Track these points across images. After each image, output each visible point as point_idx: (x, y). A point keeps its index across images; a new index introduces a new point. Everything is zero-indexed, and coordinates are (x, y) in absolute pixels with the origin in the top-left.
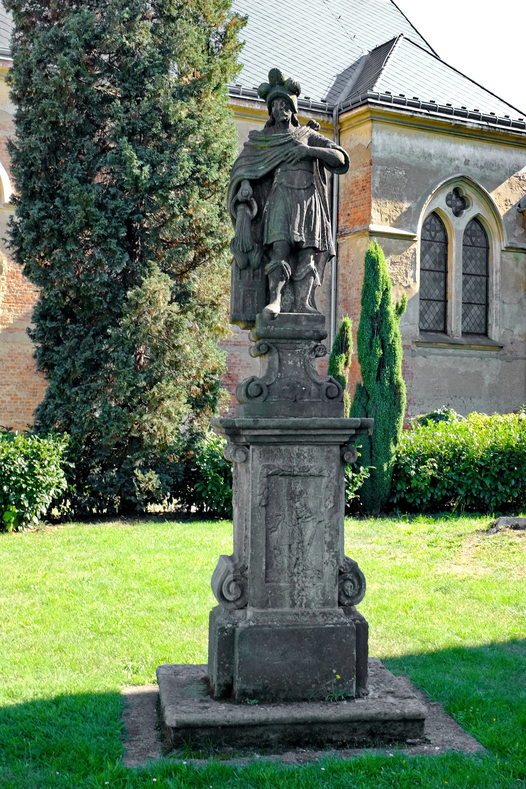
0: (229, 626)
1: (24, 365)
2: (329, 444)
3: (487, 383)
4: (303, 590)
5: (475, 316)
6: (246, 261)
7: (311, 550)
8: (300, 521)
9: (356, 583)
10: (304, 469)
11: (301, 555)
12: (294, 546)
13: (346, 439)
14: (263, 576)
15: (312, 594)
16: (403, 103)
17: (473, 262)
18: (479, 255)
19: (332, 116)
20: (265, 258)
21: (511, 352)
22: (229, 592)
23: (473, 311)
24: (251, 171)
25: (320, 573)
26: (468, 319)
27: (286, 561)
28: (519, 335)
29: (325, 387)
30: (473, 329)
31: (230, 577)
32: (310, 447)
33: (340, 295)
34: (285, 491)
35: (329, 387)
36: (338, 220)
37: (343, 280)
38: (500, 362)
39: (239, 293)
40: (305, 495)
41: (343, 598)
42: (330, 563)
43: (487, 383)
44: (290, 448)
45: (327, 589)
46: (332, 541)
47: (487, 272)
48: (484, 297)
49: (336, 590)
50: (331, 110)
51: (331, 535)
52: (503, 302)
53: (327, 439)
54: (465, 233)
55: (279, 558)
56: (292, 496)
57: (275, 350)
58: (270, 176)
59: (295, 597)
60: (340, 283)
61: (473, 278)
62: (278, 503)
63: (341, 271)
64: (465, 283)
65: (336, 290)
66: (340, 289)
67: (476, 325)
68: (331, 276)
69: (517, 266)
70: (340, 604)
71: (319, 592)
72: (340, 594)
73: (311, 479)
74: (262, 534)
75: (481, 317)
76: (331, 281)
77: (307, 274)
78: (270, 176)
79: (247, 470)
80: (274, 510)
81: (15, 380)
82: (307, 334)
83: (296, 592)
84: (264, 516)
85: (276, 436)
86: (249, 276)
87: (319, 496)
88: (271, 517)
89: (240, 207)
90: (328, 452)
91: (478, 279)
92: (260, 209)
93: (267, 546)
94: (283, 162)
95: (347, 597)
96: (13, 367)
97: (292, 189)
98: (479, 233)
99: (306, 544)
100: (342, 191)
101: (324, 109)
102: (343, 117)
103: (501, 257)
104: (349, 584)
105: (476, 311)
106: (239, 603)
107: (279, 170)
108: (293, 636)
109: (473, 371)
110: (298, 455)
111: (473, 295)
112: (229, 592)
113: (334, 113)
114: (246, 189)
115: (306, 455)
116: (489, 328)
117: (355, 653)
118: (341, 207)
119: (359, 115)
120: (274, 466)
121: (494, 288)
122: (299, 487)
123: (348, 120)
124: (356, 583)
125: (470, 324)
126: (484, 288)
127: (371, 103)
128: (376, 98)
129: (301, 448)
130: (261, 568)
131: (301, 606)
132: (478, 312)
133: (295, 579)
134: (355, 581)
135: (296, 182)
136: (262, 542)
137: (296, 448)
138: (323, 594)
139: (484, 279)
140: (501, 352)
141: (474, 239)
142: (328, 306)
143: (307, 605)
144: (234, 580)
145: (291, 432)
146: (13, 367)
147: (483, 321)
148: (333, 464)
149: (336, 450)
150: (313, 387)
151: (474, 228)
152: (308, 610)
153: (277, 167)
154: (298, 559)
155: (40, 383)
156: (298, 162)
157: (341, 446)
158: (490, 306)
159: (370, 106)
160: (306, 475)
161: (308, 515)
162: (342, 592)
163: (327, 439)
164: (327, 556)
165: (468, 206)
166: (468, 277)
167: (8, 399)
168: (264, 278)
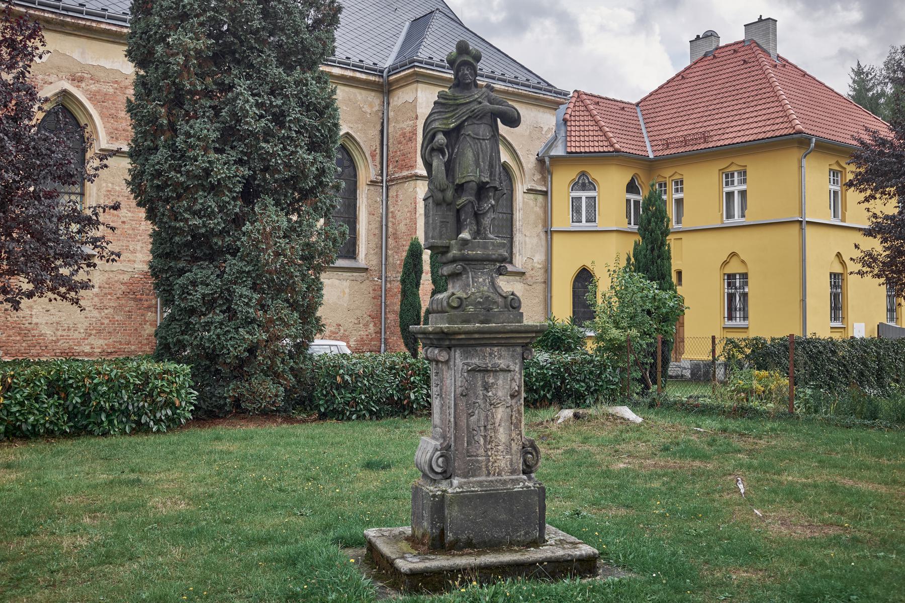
0: (439, 493)
1: (120, 291)
7: (501, 430)
10: (494, 365)
12: (489, 427)
16: (432, 65)
24: (444, 124)
29: (509, 299)
33: (390, 230)
34: (480, 383)
36: (388, 166)
44: (484, 348)
47: (512, 211)
50: (382, 72)
53: (512, 341)
56: (486, 387)
62: (475, 393)
63: (391, 209)
66: (390, 224)
78: (458, 128)
81: (112, 304)
82: (493, 257)
92: (450, 155)
94: (470, 117)
96: (110, 294)
100: (391, 141)
108: (491, 498)
113: (385, 74)
118: (391, 154)
122: (491, 380)
128: (421, 62)
131: (494, 475)
133: (490, 453)
137: (488, 349)
138: (511, 465)
139: (509, 216)
143: (499, 474)
145: (477, 336)
146: (110, 294)
150: (500, 300)
152: (500, 478)
160: (496, 371)
163: (512, 341)
167: (106, 321)
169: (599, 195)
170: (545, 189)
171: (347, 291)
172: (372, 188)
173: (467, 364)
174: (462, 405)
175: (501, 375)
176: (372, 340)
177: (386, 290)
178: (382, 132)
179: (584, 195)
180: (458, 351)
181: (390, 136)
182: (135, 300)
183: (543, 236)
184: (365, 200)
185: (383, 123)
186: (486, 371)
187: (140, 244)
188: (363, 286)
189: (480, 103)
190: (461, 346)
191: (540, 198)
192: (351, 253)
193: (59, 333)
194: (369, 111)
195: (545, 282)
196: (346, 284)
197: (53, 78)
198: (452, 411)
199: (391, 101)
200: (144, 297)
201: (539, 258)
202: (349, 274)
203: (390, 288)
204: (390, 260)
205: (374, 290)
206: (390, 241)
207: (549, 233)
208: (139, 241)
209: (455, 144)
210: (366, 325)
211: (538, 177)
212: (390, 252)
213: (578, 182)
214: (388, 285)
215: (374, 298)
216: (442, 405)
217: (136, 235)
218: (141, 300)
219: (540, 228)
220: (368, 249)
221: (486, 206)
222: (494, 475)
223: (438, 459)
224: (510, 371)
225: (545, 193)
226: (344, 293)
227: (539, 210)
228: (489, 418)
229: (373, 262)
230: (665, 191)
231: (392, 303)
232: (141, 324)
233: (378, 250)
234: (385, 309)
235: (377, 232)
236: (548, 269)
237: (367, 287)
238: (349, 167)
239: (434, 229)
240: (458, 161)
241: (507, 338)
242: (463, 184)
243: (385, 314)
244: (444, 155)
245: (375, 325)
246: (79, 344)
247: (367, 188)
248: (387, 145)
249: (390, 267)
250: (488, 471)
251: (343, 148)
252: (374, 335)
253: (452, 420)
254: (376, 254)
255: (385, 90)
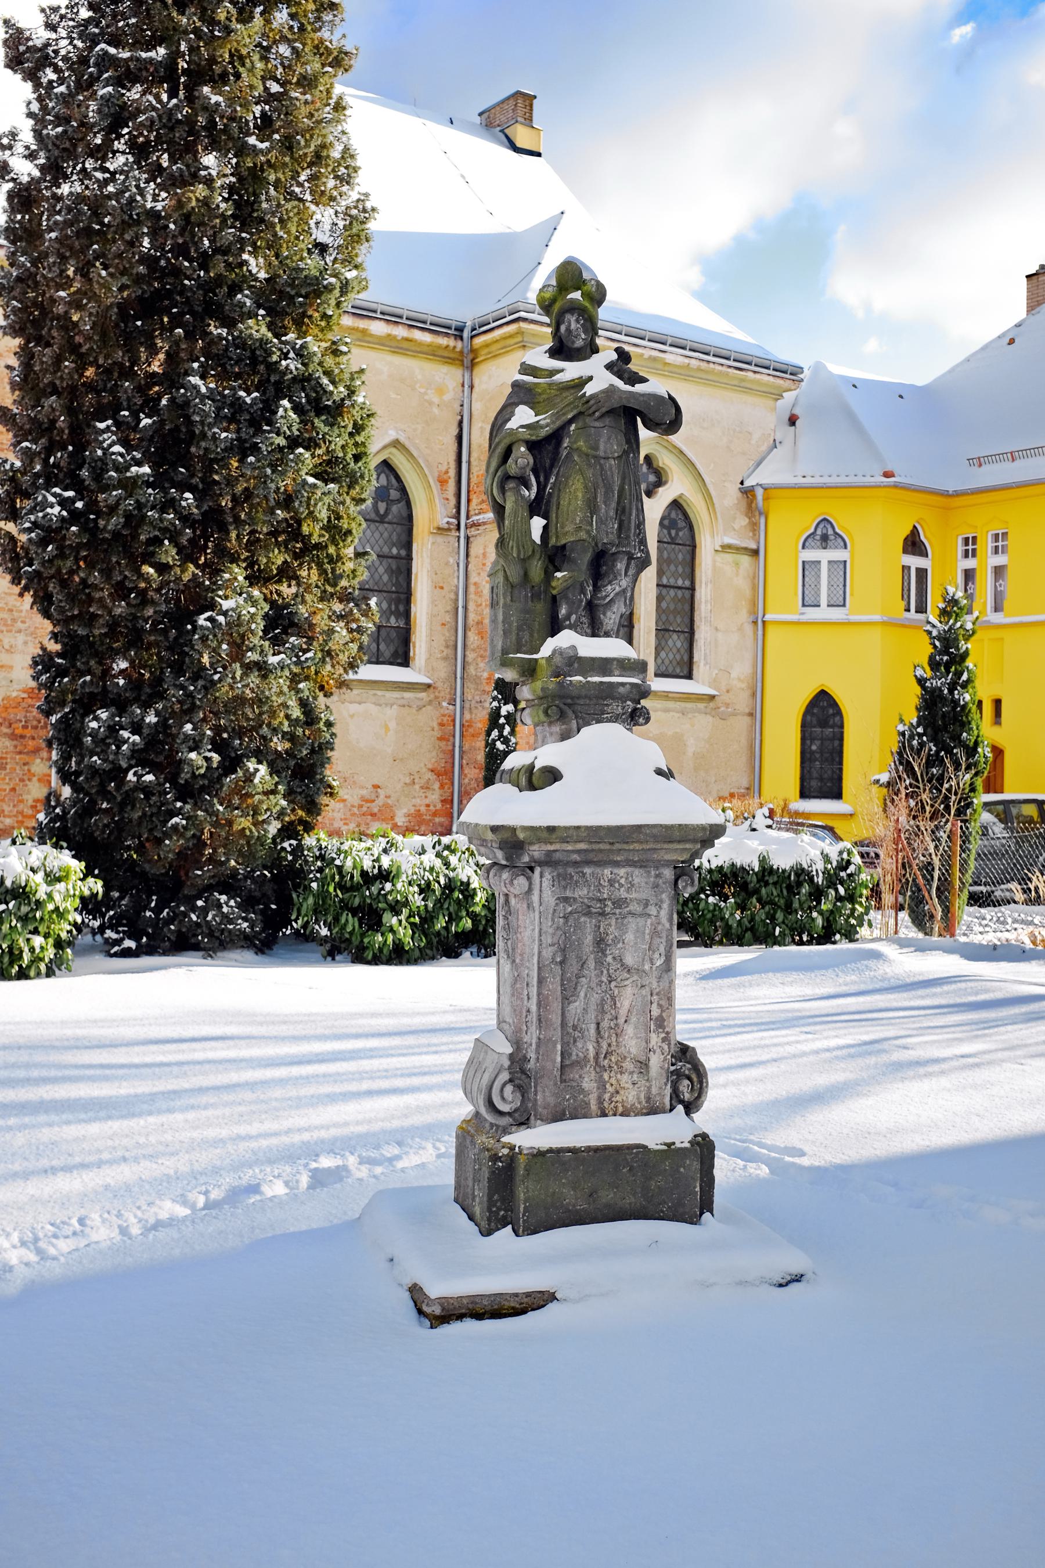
2: (659, 864)
3: (690, 751)
4: (617, 1092)
5: (675, 650)
6: (522, 573)
7: (630, 1030)
8: (613, 984)
9: (695, 1079)
11: (614, 1039)
12: (605, 1024)
17: (672, 567)
18: (680, 556)
19: (462, 338)
20: (551, 567)
21: (727, 705)
22: (503, 1098)
23: (670, 643)
25: (643, 1066)
26: (663, 654)
27: (591, 1048)
28: (739, 679)
30: (670, 669)
31: (505, 1076)
32: (629, 869)
33: (472, 616)
36: (469, 501)
37: (476, 593)
39: (510, 624)
40: (620, 945)
42: (658, 1051)
43: (690, 751)
44: (598, 870)
45: (654, 1091)
46: (661, 1016)
48: (687, 620)
49: (668, 1090)
51: (660, 1006)
52: (716, 629)
54: (661, 524)
55: (579, 1045)
57: (570, 713)
59: (606, 1105)
60: (472, 596)
61: (672, 592)
64: (660, 599)
65: (466, 608)
66: (471, 606)
67: (674, 663)
68: (457, 587)
69: (737, 575)
71: (642, 1096)
73: (630, 919)
74: (556, 1006)
75: (682, 651)
76: (457, 595)
77: (617, 594)
79: (530, 906)
83: (607, 1096)
84: (558, 978)
85: (578, 852)
86: (526, 596)
87: (632, 941)
89: (511, 485)
91: (680, 593)
92: (541, 488)
93: (564, 1024)
94: (581, 413)
97: (595, 457)
98: (681, 524)
99: (621, 1021)
100: (474, 455)
101: (449, 328)
102: (479, 341)
103: (714, 561)
104: (686, 1082)
105: (676, 642)
107: (573, 427)
109: (670, 733)
110: (611, 882)
111: (671, 617)
112: (503, 1098)
113: (466, 334)
114: (522, 458)
115: (623, 881)
116: (695, 667)
117: (698, 1189)
119: (505, 338)
120: (575, 899)
121: (703, 606)
123: (487, 345)
124: (695, 1079)
125: (667, 662)
126: (687, 607)
127: (525, 320)
129: (615, 871)
130: (554, 1061)
132: (679, 644)
134: (694, 1077)
135: (602, 447)
136: (556, 1019)
137: (607, 872)
139: (687, 593)
140: (712, 705)
141: (673, 532)
142: (453, 632)
144: (511, 1081)
147: (686, 658)
148: (664, 896)
151: (673, 515)
153: (570, 422)
154: (609, 1045)
155: (12, 748)
156: (602, 416)
158: (696, 636)
159: (522, 324)
161: (626, 975)
164: (655, 1039)
165: (666, 482)
166: (664, 591)
168: (549, 598)
169: (852, 557)
170: (754, 546)
171: (392, 725)
172: (440, 539)
173: (566, 900)
174: (554, 985)
176: (435, 814)
177: (462, 726)
178: (459, 438)
179: (824, 556)
180: (547, 876)
181: (474, 446)
182: (13, 737)
183: (749, 629)
184: (427, 561)
185: (461, 423)
187: (21, 638)
191: (745, 560)
194: (436, 400)
195: (751, 715)
196: (392, 712)
198: (534, 991)
199: (476, 382)
200: (28, 733)
201: (741, 670)
203: (470, 721)
204: (471, 670)
205: (441, 725)
206: (472, 636)
207: (760, 624)
208: (20, 631)
209: (552, 466)
210: (426, 787)
211: (743, 521)
212: (471, 656)
213: (814, 534)
214: (467, 716)
215: (440, 739)
216: (516, 980)
217: (14, 620)
218: (22, 737)
219: (743, 616)
223: (504, 1085)
225: (755, 553)
226: (387, 728)
227: (742, 583)
228: (608, 1004)
230: (974, 550)
231: (473, 749)
232: (22, 780)
233: (449, 652)
234: (461, 758)
235: (448, 618)
236: (757, 690)
238: (399, 501)
239: (506, 633)
240: (554, 500)
242: (564, 547)
243: (461, 767)
245: (442, 787)
247: (431, 539)
248: (469, 462)
249: (470, 686)
251: (386, 466)
252: (439, 806)
253: (534, 1008)
254: (445, 659)
255: (467, 362)
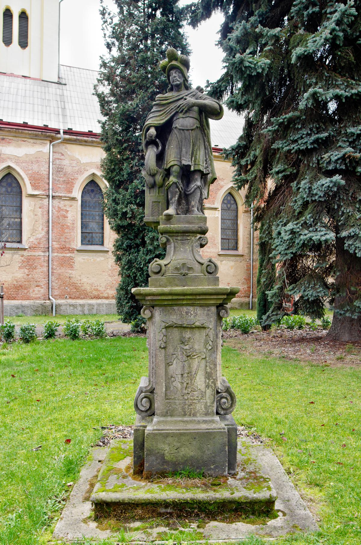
2: (208, 305)
12: (185, 375)
13: (221, 302)
14: (163, 395)
15: (197, 407)
22: (142, 405)
35: (208, 265)
38: (71, 247)
41: (220, 409)
58: (169, 123)
70: (218, 413)
71: (203, 406)
72: (217, 407)
78: (169, 123)
80: (170, 350)
88: (169, 355)
90: (208, 310)
95: (223, 409)
106: (149, 412)
115: (192, 312)
134: (229, 398)
149: (214, 309)
154: (187, 384)
157: (217, 307)
162: (219, 405)
172: (245, 214)
175: (197, 332)
186: (182, 327)
188: (241, 264)
189: (185, 99)
190: (160, 306)
192: (236, 248)
193: (94, 288)
196: (232, 263)
197: (88, 168)
202: (233, 258)
214: (254, 263)
220: (243, 245)
221: (193, 186)
222: (190, 415)
224: (204, 328)
229: (246, 251)
237: (243, 264)
241: (173, 300)
244: (157, 147)
246: (102, 293)
250: (185, 412)
